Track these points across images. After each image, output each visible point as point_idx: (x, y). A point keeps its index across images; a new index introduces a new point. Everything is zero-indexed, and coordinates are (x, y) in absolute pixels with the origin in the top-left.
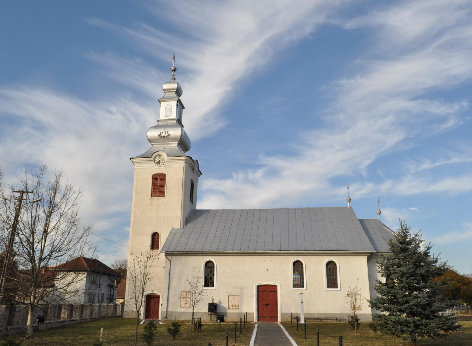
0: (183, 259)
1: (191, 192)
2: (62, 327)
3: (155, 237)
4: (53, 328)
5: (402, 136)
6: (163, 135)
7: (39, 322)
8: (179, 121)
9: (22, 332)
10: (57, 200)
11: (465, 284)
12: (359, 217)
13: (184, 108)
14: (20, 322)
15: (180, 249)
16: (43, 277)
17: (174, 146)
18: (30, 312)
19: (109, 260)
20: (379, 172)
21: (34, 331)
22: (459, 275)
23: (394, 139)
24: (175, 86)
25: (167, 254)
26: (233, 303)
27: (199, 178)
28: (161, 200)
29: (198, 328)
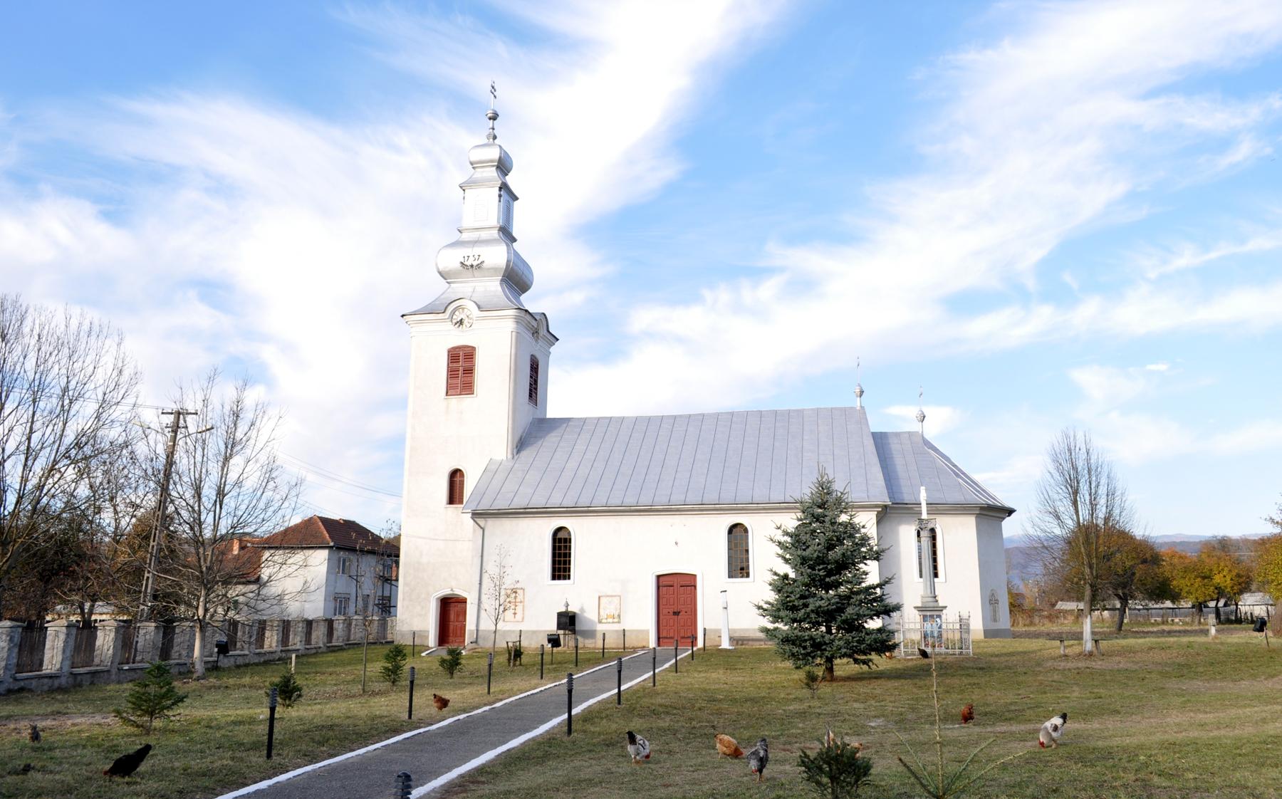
0: (507, 523)
1: (533, 381)
2: (266, 663)
3: (456, 477)
4: (247, 665)
5: (1121, 188)
6: (468, 263)
7: (219, 653)
8: (506, 233)
9: (186, 671)
10: (239, 435)
11: (1144, 561)
12: (875, 427)
13: (516, 198)
14: (184, 653)
15: (501, 504)
16: (239, 560)
17: (493, 287)
18: (198, 635)
19: (376, 524)
20: (1067, 278)
21: (207, 670)
22: (1132, 538)
23: (1099, 197)
24: (494, 154)
25: (476, 515)
26: (608, 612)
27: (552, 349)
28: (466, 401)
29: (515, 660)
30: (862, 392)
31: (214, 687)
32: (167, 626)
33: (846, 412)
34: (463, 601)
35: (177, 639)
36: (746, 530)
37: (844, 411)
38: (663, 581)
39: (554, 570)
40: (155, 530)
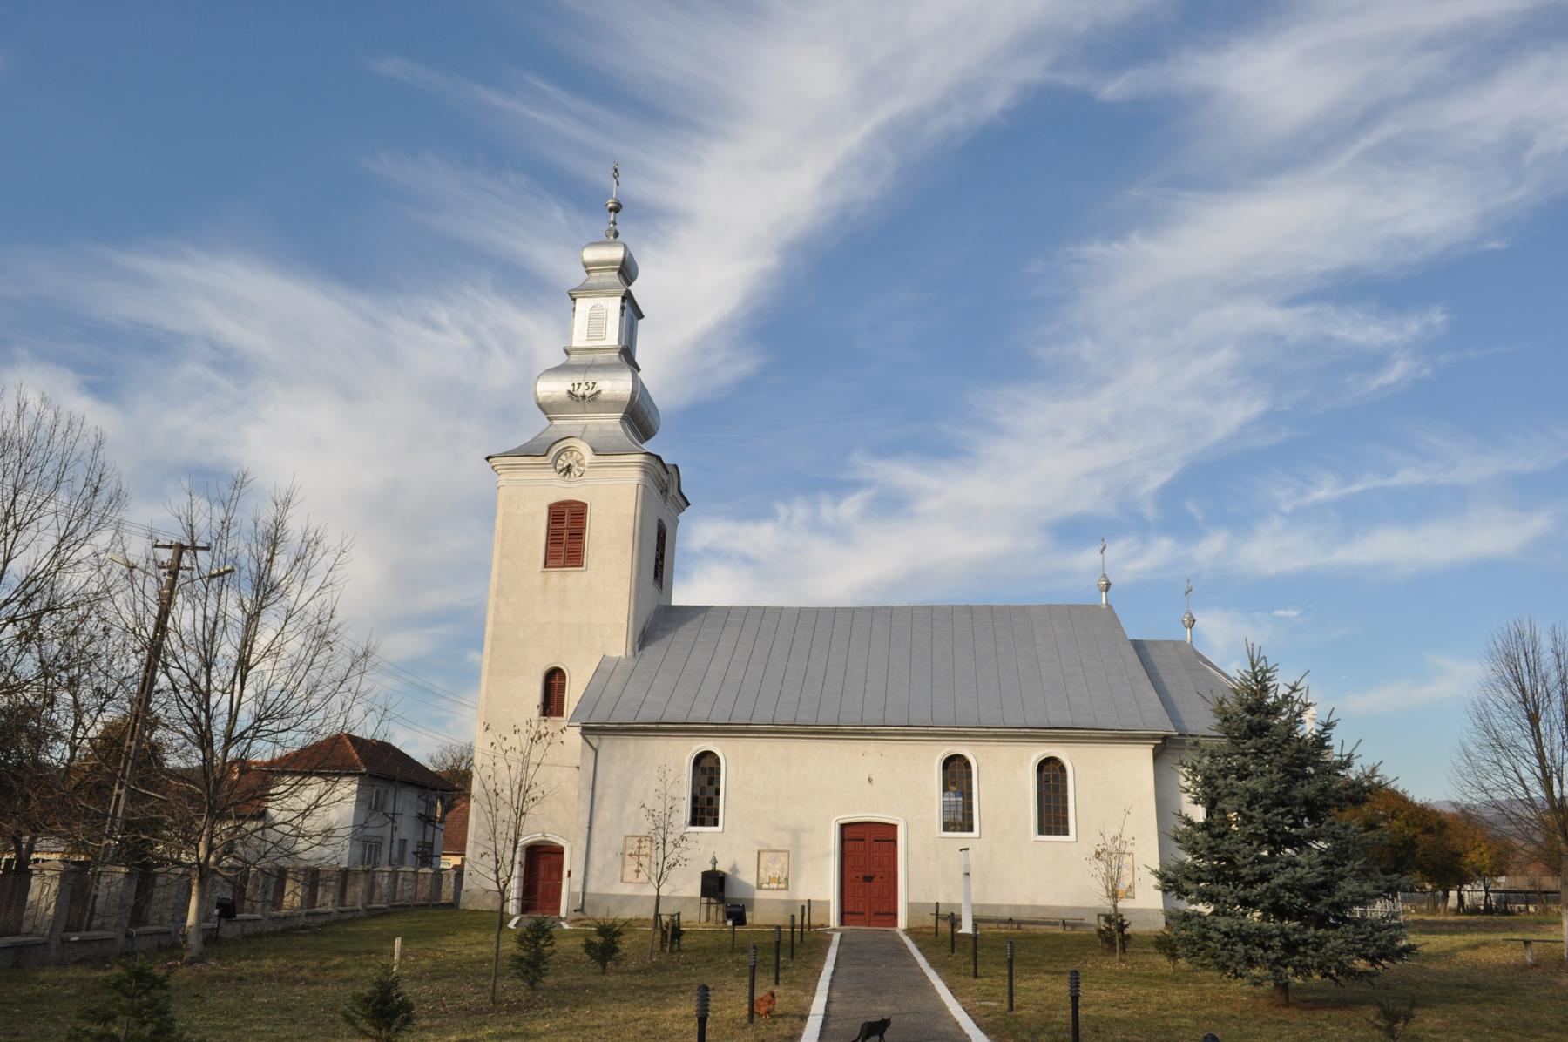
0: (632, 744)
1: (658, 556)
3: (554, 681)
5: (1258, 407)
6: (580, 392)
7: (220, 916)
8: (627, 354)
9: (172, 944)
10: (278, 572)
12: (1133, 634)
13: (641, 316)
14: (168, 915)
15: (623, 717)
16: (236, 790)
17: (611, 423)
18: (195, 888)
19: (423, 746)
20: (1191, 506)
23: (1236, 414)
24: (617, 253)
25: (587, 731)
26: (770, 873)
28: (572, 576)
30: (1109, 585)
31: (219, 977)
32: (144, 874)
33: (1090, 611)
34: (559, 851)
35: (159, 894)
36: (968, 765)
37: (1083, 609)
38: (850, 833)
39: (694, 811)
40: (128, 750)
